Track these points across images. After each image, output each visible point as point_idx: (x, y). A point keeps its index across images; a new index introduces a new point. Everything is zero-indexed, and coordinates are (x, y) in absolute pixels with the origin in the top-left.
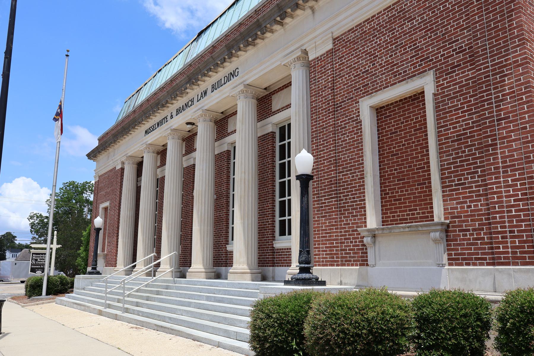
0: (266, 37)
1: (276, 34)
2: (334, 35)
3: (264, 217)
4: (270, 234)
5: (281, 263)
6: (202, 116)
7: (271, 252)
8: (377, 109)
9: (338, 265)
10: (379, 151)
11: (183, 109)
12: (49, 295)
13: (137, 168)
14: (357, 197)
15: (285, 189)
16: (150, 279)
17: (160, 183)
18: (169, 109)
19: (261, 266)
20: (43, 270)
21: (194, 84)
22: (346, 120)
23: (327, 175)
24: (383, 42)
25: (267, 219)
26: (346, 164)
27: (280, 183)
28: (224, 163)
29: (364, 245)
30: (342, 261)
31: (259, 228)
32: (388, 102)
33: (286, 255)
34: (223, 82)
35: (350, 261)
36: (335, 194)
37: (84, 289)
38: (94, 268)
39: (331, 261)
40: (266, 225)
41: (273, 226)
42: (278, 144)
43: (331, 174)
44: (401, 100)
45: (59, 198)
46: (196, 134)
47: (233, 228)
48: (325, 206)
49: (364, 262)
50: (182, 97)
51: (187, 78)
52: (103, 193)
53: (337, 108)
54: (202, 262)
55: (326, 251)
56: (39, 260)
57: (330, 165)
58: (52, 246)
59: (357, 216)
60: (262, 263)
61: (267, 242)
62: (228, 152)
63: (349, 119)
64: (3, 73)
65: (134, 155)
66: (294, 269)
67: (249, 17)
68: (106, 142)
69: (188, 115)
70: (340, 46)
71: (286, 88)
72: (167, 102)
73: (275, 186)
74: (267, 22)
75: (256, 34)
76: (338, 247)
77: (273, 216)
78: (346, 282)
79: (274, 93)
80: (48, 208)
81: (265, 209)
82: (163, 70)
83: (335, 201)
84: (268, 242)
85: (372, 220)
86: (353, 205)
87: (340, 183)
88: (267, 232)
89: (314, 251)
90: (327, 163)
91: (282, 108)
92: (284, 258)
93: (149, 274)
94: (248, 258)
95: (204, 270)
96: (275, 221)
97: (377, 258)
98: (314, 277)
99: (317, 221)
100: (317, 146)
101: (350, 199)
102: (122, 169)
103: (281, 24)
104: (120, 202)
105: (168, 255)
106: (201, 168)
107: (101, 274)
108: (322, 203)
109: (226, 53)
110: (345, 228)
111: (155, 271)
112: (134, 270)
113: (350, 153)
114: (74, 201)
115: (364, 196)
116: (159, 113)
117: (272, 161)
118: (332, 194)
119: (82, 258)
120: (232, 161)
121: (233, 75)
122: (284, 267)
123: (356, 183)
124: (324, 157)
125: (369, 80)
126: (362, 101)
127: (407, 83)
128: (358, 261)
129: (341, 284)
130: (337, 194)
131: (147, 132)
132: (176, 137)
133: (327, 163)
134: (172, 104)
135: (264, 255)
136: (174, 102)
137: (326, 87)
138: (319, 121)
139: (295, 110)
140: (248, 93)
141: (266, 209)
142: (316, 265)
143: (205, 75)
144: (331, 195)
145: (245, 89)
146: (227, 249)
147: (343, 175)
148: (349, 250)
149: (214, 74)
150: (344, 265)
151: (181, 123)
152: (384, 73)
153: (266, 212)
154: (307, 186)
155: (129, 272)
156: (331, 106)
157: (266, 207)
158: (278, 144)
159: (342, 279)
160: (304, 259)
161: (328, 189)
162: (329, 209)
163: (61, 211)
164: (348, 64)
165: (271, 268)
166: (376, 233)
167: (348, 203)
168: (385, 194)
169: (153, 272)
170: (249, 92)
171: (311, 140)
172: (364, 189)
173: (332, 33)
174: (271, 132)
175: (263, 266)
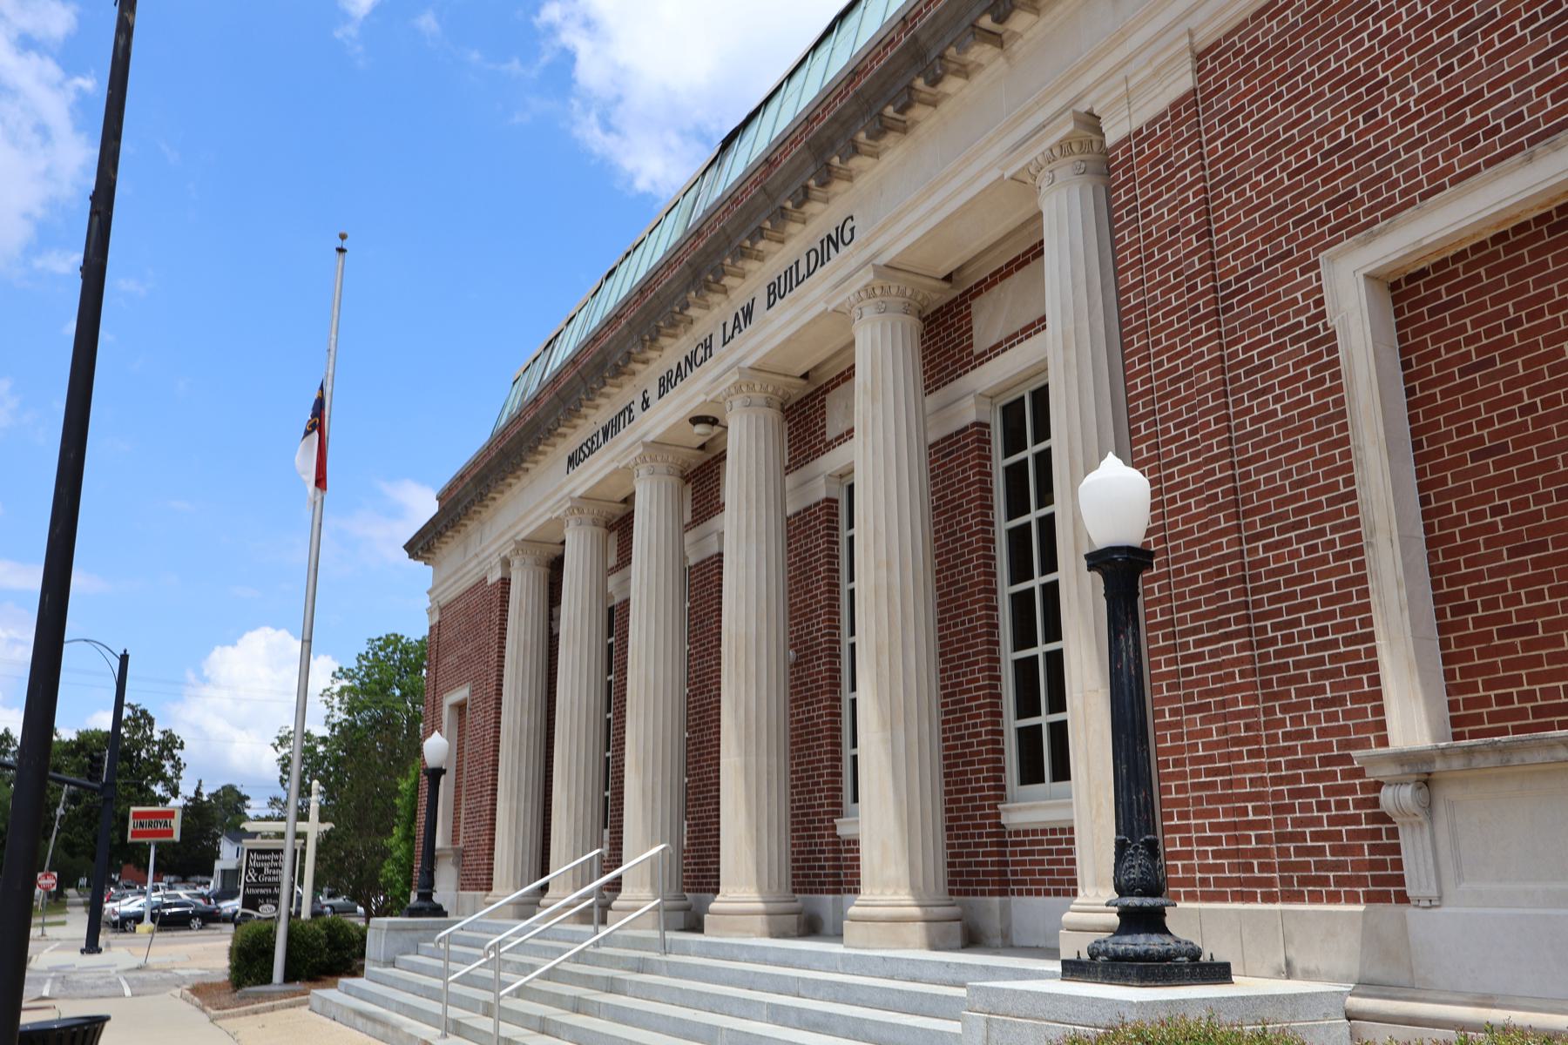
0: (946, 95)
1: (979, 79)
2: (1197, 38)
3: (961, 719)
4: (985, 779)
5: (1033, 882)
6: (738, 389)
7: (992, 844)
8: (1394, 286)
9: (1269, 898)
10: (1417, 445)
11: (680, 374)
13: (550, 576)
14: (1337, 629)
15: (1039, 616)
16: (590, 936)
17: (615, 619)
18: (637, 380)
19: (959, 893)
20: (275, 898)
21: (710, 290)
22: (1266, 340)
23: (1203, 553)
24: (1406, 27)
25: (975, 725)
26: (1279, 504)
27: (1014, 596)
28: (816, 547)
29: (1384, 818)
30: (1286, 881)
31: (946, 758)
32: (1438, 252)
33: (1050, 852)
34: (803, 270)
35: (1324, 881)
36: (1238, 620)
37: (392, 963)
38: (426, 896)
39: (1239, 882)
40: (970, 745)
41: (994, 751)
42: (999, 464)
44: (1500, 238)
45: (357, 682)
46: (722, 457)
47: (855, 758)
48: (1200, 669)
49: (1386, 885)
50: (674, 336)
52: (451, 659)
53: (1225, 299)
56: (267, 871)
57: (1211, 511)
58: (302, 826)
59: (1340, 701)
60: (963, 883)
61: (975, 808)
62: (831, 503)
63: (1277, 335)
64: (85, 261)
66: (1094, 904)
67: (882, 44)
68: (456, 501)
69: (692, 394)
70: (1223, 75)
71: (1018, 268)
72: (629, 357)
73: (995, 609)
74: (947, 41)
75: (910, 88)
76: (1265, 825)
77: (993, 714)
78: (1312, 966)
79: (980, 292)
80: (328, 712)
82: (621, 271)
83: (1241, 648)
85: (1411, 718)
86: (1321, 661)
88: (973, 772)
90: (1198, 504)
92: (1041, 862)
93: (584, 917)
94: (911, 865)
95: (761, 906)
96: (1001, 733)
97: (1448, 872)
98: (1184, 948)
99: (1169, 725)
101: (1305, 635)
102: (505, 582)
103: (997, 40)
104: (500, 685)
105: (646, 850)
106: (742, 561)
107: (445, 914)
108: (1186, 659)
109: (812, 170)
111: (606, 907)
112: (543, 902)
113: (1290, 460)
114: (397, 692)
115: (1368, 622)
116: (608, 396)
117: (983, 522)
118: (1227, 623)
119: (397, 861)
120: (844, 534)
121: (834, 241)
123: (1329, 573)
124: (1185, 483)
125: (1356, 178)
126: (1331, 259)
127: (1530, 159)
128: (1360, 881)
129: (1289, 972)
130: (1247, 618)
131: (573, 461)
133: (1198, 504)
135: (969, 855)
136: (652, 354)
137: (1177, 229)
138: (1157, 354)
139: (1064, 338)
140: (889, 293)
141: (969, 691)
143: (744, 254)
144: (1221, 624)
146: (1003, 821)
147: (1266, 548)
148: (1316, 836)
149: (774, 246)
150: (1297, 897)
151: (672, 421)
152: (1422, 141)
153: (969, 700)
155: (526, 908)
156: (1203, 294)
157: (969, 682)
158: (999, 464)
159: (1292, 953)
160: (1135, 874)
161: (1208, 602)
162: (1216, 680)
163: (363, 720)
164: (1260, 133)
165: (997, 899)
166: (1439, 765)
167: (1299, 651)
168: (1456, 611)
169: (596, 911)
170: (894, 291)
172: (1365, 593)
173: (1191, 34)
174: (975, 424)
175: (967, 893)
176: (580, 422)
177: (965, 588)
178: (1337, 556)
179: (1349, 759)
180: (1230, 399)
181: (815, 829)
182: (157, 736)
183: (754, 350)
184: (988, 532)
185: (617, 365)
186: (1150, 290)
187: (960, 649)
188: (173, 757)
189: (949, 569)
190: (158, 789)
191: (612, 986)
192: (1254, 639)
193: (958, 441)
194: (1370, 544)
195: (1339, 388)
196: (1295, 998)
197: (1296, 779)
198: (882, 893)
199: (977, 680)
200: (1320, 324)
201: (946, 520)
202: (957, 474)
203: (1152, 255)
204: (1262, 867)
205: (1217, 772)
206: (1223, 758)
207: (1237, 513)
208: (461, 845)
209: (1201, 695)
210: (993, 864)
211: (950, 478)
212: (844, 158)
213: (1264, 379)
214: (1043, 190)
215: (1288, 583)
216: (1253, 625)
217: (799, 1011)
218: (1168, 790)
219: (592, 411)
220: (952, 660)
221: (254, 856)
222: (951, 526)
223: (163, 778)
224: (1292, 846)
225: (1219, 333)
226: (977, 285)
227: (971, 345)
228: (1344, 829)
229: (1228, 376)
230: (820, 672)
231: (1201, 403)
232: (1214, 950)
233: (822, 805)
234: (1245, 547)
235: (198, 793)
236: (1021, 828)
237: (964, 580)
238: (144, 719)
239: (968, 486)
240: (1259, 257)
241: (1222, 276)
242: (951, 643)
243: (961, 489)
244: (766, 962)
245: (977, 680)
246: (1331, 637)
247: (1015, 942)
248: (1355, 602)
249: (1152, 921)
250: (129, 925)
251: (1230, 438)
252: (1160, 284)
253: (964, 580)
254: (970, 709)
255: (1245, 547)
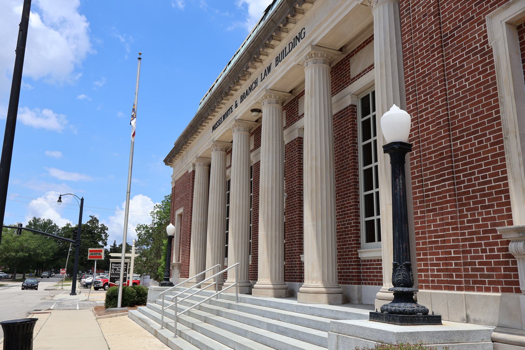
3: (345, 218)
4: (353, 240)
5: (370, 280)
6: (266, 98)
7: (355, 265)
8: (519, 27)
9: (460, 289)
11: (247, 94)
12: (125, 306)
14: (491, 175)
18: (234, 97)
19: (343, 283)
21: (256, 61)
25: (349, 220)
29: (511, 256)
30: (467, 282)
31: (338, 232)
34: (287, 51)
35: (484, 283)
36: (448, 174)
37: (155, 302)
39: (448, 282)
40: (348, 227)
42: (360, 120)
43: (441, 144)
49: (511, 284)
50: (245, 80)
51: (248, 55)
53: (445, 41)
54: (269, 275)
55: (438, 265)
56: (118, 270)
57: (438, 129)
59: (492, 206)
61: (349, 251)
63: (467, 53)
65: (204, 155)
66: (384, 293)
71: (367, 44)
72: (230, 89)
73: (358, 176)
76: (459, 258)
78: (478, 318)
79: (353, 55)
80: (153, 219)
81: (345, 207)
83: (450, 185)
84: (351, 251)
86: (484, 190)
87: (457, 155)
89: (417, 266)
91: (363, 72)
92: (373, 272)
94: (323, 272)
95: (271, 286)
96: (359, 223)
98: (420, 309)
99: (420, 218)
100: (416, 104)
101: (477, 179)
102: (194, 172)
106: (267, 160)
108: (427, 190)
109: (289, 11)
110: (471, 227)
115: (504, 172)
116: (224, 104)
117: (353, 143)
121: (298, 39)
122: (373, 286)
126: (491, 18)
128: (500, 283)
129: (467, 320)
130: (452, 173)
131: (214, 128)
132: (242, 128)
133: (433, 127)
134: (236, 90)
136: (238, 87)
138: (417, 67)
139: (381, 70)
141: (347, 207)
142: (421, 287)
143: (267, 46)
144: (442, 176)
145: (313, 52)
146: (359, 256)
147: (461, 143)
148: (480, 263)
149: (277, 43)
150: (472, 289)
151: (245, 111)
153: (348, 210)
154: (403, 162)
158: (360, 120)
159: (469, 312)
160: (401, 278)
161: (436, 167)
162: (439, 198)
165: (356, 286)
167: (474, 185)
170: (319, 55)
171: (405, 98)
172: (504, 160)
174: (351, 105)
175: (346, 283)
176: (216, 114)
177: (346, 168)
178: (492, 145)
179: (496, 231)
180: (447, 82)
181: (293, 258)
182: (100, 226)
183: (271, 82)
184: (355, 146)
185: (226, 92)
186: (415, 41)
187: (344, 191)
188: (105, 233)
189: (341, 161)
190: (100, 243)
191: (218, 313)
192: (455, 181)
193: (345, 112)
194: (506, 138)
195: (494, 72)
196: (469, 332)
197: (472, 239)
198: (312, 283)
199: (350, 203)
200: (486, 46)
201: (340, 143)
202: (344, 125)
203: (416, 26)
204: (457, 276)
205: (439, 237)
206: (441, 231)
207: (449, 129)
208: (180, 262)
209: (433, 205)
210: (355, 272)
211: (341, 126)
212: (300, 5)
213: (461, 73)
214: (374, 6)
215: (470, 157)
216: (455, 175)
217: (277, 326)
218: (415, 243)
219: (219, 110)
220: (341, 195)
221: (113, 265)
222: (342, 145)
223: (102, 239)
224: (470, 267)
225: (443, 55)
226: (352, 52)
227: (350, 75)
228: (492, 261)
229: (446, 73)
230: (295, 201)
231: (435, 85)
232: (433, 310)
233: (295, 250)
234: (452, 143)
235: (114, 244)
236: (366, 259)
237: (346, 165)
238: (94, 221)
239: (348, 129)
240: (459, 21)
241: (444, 31)
242: (341, 189)
243: (345, 130)
244: (271, 307)
245: (350, 203)
246: (488, 179)
247: (363, 303)
248: (499, 164)
249: (409, 297)
250: (89, 286)
251: (446, 98)
252: (419, 38)
253: (346, 165)
254: (347, 214)
255: (452, 143)
